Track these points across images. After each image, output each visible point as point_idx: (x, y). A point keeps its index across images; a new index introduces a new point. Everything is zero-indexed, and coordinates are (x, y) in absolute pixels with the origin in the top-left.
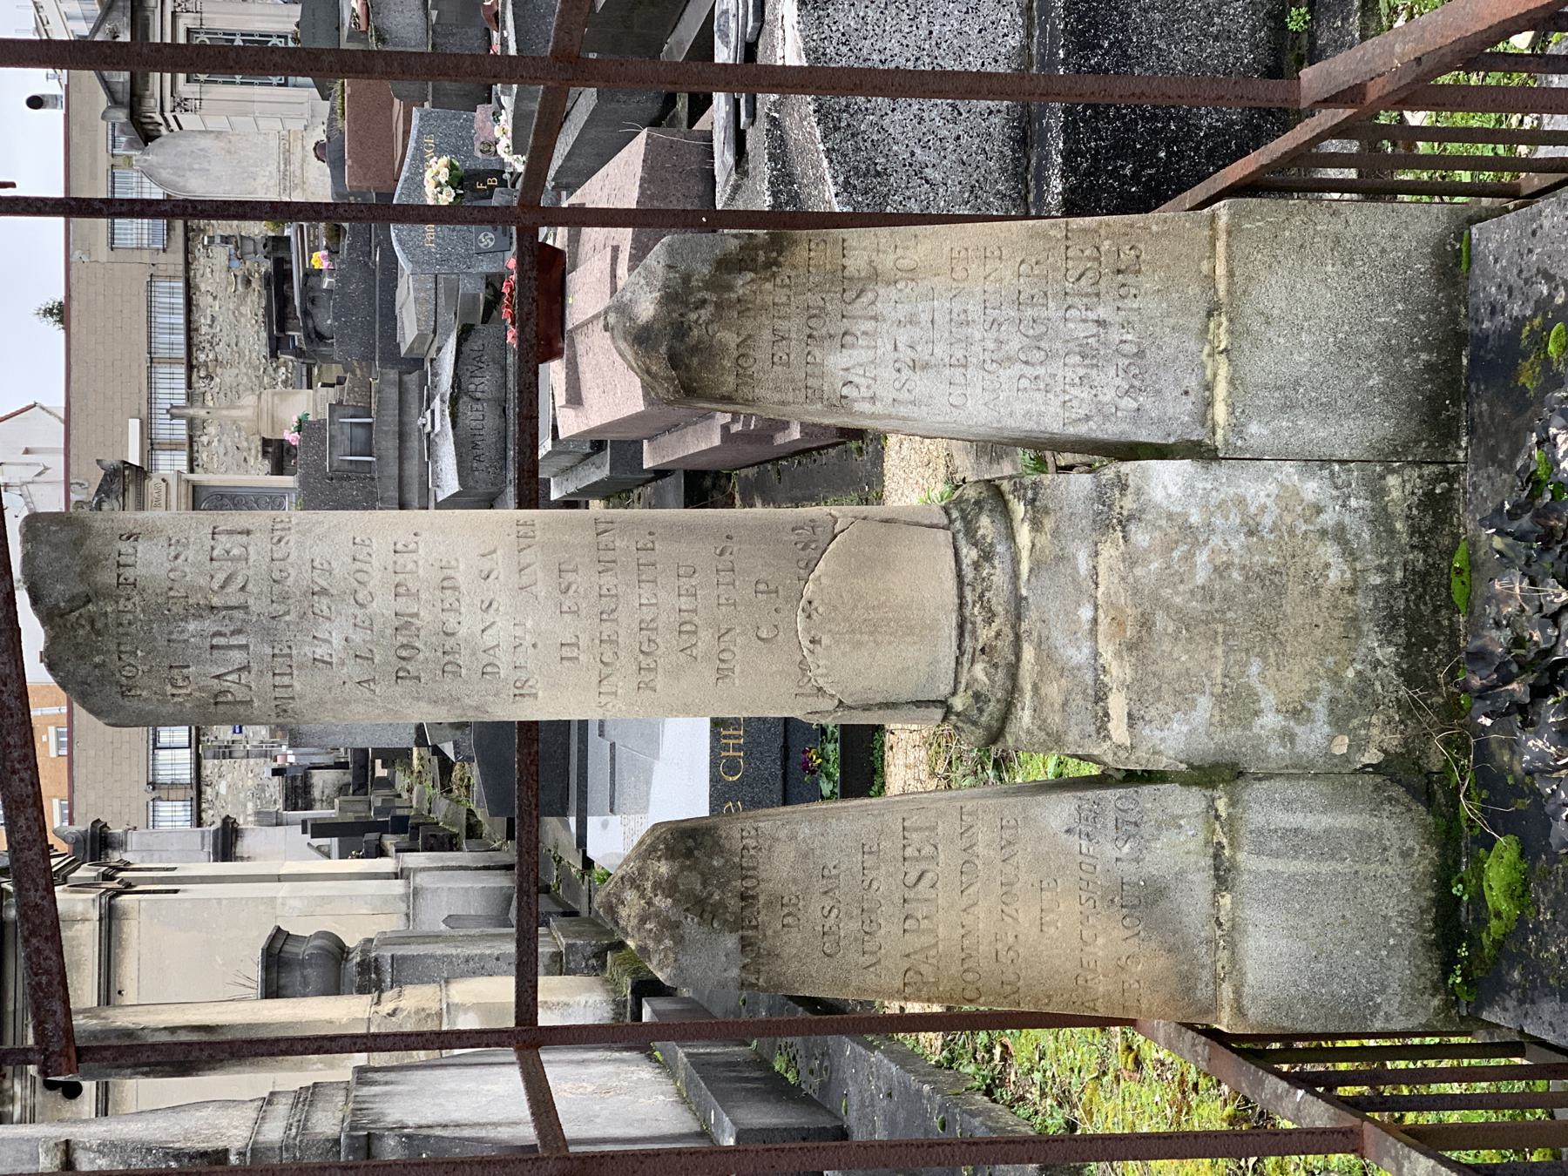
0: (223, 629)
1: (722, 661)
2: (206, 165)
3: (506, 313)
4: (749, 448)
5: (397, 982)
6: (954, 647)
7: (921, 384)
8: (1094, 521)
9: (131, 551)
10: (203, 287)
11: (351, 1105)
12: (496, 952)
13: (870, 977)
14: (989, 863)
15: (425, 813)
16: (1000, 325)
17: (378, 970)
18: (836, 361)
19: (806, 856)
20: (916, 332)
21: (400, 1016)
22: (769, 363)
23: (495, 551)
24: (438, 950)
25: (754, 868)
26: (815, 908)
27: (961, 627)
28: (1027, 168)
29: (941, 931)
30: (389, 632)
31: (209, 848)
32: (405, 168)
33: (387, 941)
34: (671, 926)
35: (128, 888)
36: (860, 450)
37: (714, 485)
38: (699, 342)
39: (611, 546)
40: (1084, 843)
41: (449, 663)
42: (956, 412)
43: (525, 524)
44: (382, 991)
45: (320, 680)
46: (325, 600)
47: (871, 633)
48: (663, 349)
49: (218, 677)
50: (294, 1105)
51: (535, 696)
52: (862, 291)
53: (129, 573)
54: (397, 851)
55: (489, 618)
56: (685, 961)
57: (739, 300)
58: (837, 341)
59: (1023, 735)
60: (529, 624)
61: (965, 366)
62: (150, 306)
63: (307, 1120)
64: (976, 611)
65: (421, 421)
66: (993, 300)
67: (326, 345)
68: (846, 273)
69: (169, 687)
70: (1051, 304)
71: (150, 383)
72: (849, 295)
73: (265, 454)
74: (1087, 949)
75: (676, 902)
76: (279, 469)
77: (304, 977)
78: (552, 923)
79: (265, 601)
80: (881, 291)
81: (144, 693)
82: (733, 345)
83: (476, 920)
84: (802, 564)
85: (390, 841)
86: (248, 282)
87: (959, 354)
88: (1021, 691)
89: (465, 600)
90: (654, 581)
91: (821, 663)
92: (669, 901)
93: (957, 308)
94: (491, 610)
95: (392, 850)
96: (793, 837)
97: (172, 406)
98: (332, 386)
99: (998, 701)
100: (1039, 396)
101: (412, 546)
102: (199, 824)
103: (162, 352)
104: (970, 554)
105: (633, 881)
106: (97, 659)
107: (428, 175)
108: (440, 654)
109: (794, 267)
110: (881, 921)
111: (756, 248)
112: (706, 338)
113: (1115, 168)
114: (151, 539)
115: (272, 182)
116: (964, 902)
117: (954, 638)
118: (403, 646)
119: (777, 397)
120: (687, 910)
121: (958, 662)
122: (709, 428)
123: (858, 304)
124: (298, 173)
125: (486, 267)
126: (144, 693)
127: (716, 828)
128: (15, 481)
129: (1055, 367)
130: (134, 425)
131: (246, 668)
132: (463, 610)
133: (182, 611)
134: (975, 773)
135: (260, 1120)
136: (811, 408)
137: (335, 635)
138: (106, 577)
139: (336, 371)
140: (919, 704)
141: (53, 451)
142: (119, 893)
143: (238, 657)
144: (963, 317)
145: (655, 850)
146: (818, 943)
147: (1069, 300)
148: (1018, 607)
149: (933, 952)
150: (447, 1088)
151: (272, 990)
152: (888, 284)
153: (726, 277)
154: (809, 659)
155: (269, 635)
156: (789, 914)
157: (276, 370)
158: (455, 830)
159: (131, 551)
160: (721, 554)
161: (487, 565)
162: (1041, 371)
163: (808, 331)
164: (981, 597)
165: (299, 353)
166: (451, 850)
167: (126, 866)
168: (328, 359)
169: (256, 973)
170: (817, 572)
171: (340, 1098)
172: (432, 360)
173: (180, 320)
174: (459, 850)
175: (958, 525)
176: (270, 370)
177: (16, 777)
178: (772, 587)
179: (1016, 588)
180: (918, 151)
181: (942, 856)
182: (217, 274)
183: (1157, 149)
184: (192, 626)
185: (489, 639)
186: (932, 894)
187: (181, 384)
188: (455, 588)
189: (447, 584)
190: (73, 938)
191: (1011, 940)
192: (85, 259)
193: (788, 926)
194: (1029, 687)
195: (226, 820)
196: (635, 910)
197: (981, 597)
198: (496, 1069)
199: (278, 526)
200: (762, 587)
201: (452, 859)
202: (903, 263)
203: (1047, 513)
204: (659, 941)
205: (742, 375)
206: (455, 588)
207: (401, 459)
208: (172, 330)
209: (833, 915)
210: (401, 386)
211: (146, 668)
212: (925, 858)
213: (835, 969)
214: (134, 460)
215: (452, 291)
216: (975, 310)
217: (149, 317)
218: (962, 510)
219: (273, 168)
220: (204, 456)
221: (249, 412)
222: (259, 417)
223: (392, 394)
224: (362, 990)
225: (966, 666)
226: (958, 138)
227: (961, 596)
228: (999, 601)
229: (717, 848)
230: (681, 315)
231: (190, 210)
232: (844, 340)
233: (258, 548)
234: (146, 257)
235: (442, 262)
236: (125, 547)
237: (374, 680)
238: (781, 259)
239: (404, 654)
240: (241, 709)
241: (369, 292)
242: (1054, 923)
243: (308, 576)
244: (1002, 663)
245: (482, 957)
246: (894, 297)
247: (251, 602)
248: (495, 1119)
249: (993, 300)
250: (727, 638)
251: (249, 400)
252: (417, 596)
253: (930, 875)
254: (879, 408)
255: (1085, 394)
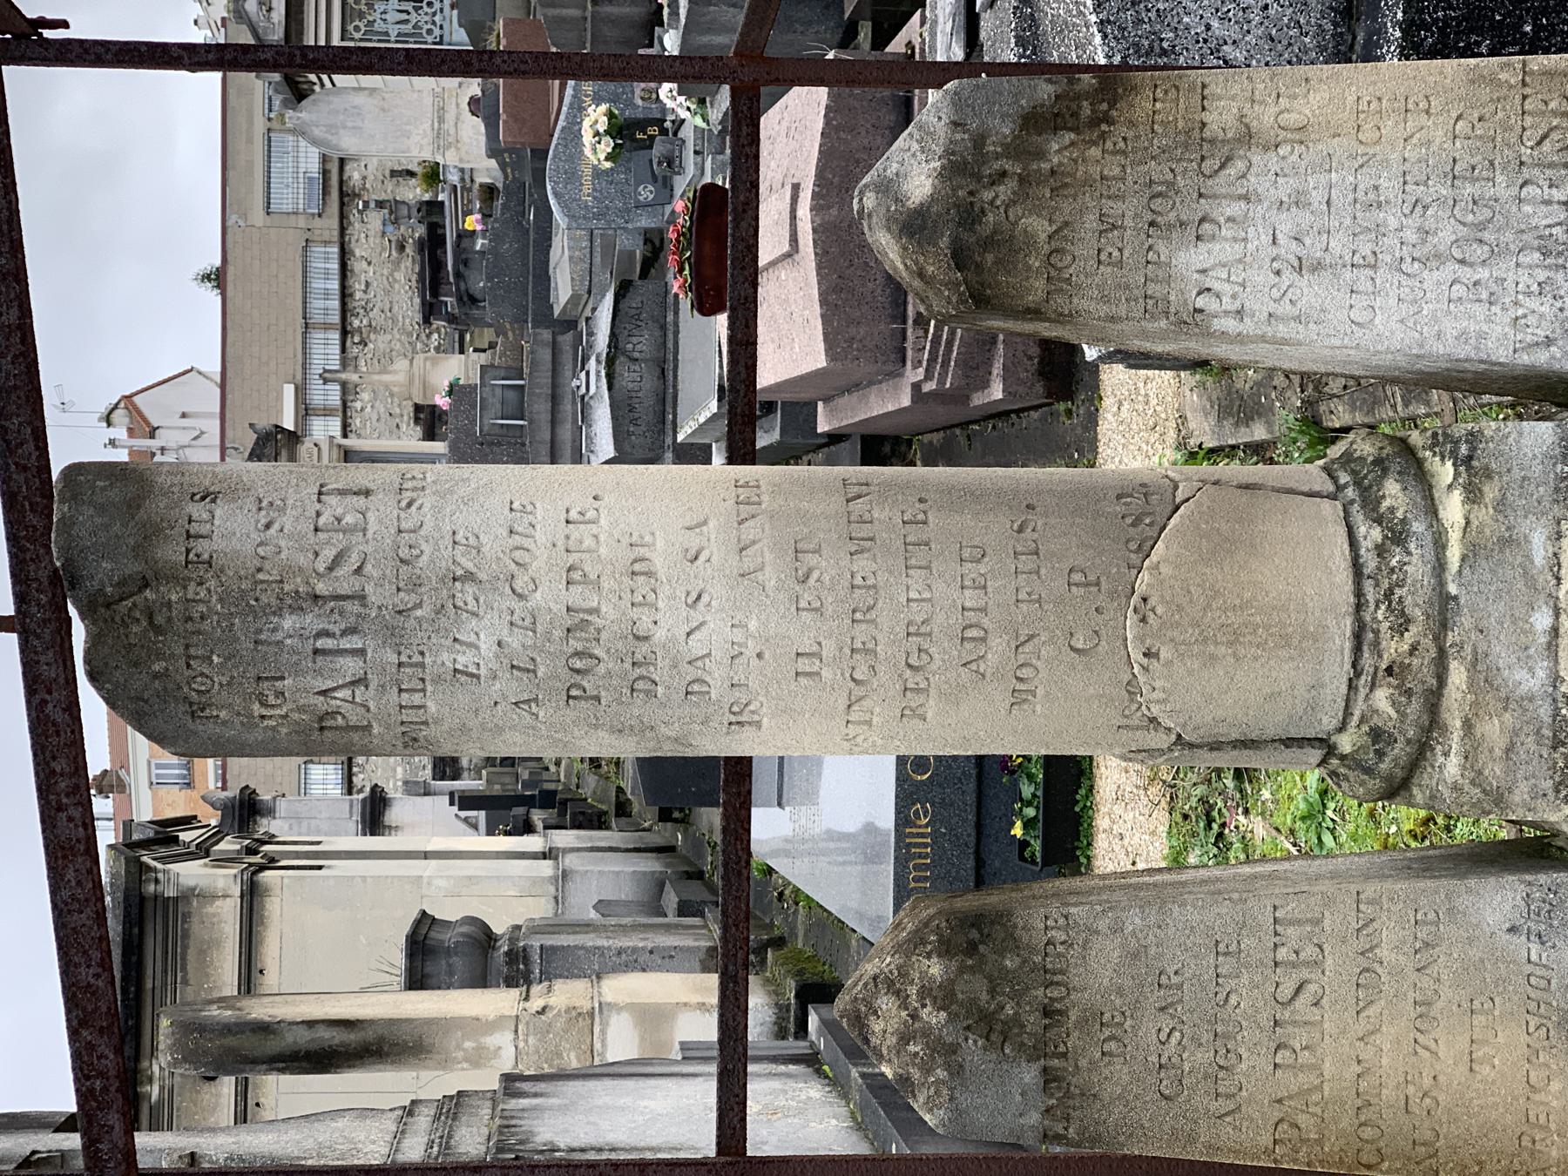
0: (331, 627)
1: (1019, 679)
2: (359, 124)
3: (671, 260)
4: (940, 410)
5: (548, 976)
6: (1348, 666)
7: (1309, 292)
8: (1557, 490)
9: (205, 516)
10: (358, 253)
11: (498, 1121)
12: (650, 945)
13: (1226, 1130)
14: (1397, 973)
15: (573, 787)
16: (1425, 208)
17: (526, 960)
18: (1189, 259)
19: (1136, 956)
20: (1305, 218)
21: (550, 1014)
22: (1093, 262)
23: (705, 523)
24: (590, 940)
25: (1062, 972)
26: (1149, 1029)
27: (1358, 637)
28: (1352, 47)
29: (1328, 1068)
30: (558, 633)
31: (357, 817)
32: (562, 117)
33: (538, 929)
34: (944, 1051)
35: (271, 863)
36: (1069, 413)
37: (893, 451)
38: (995, 232)
39: (867, 517)
40: (1535, 948)
41: (641, 678)
42: (1359, 332)
43: (747, 485)
44: (529, 983)
45: (463, 698)
46: (470, 589)
47: (1230, 644)
48: (944, 242)
49: (324, 693)
50: (436, 1118)
51: (758, 724)
52: (1229, 159)
53: (202, 547)
54: (546, 828)
55: (696, 617)
56: (964, 1100)
57: (1053, 172)
58: (1191, 231)
59: (1446, 793)
60: (753, 625)
61: (1374, 267)
62: (305, 272)
63: (450, 1137)
64: (1380, 615)
65: (575, 383)
66: (1416, 173)
67: (478, 308)
68: (1207, 134)
69: (256, 707)
70: (1500, 179)
71: (304, 348)
72: (1210, 165)
73: (417, 420)
74: (1537, 1097)
75: (953, 1017)
76: (430, 435)
77: (450, 965)
78: (708, 915)
79: (390, 588)
80: (1256, 159)
81: (223, 714)
82: (1043, 236)
83: (626, 903)
84: (1133, 546)
85: (537, 817)
86: (401, 248)
87: (1366, 250)
88: (1444, 730)
89: (664, 591)
90: (928, 568)
91: (1157, 684)
92: (943, 1015)
93: (1365, 182)
94: (701, 605)
95: (540, 825)
96: (1117, 929)
97: (326, 371)
98: (484, 351)
99: (1409, 742)
100: (1480, 310)
101: (591, 514)
102: (350, 793)
103: (316, 317)
104: (1371, 535)
105: (890, 983)
106: (157, 667)
107: (586, 123)
108: (627, 666)
109: (1132, 124)
110: (1242, 1051)
111: (1078, 97)
112: (1006, 226)
113: (1468, 45)
114: (234, 500)
115: (425, 142)
116: (1361, 1028)
117: (1347, 652)
118: (577, 654)
119: (1104, 310)
120: (968, 1028)
121: (1351, 686)
122: (897, 388)
123: (1222, 178)
124: (452, 131)
125: (645, 221)
126: (223, 714)
127: (1010, 914)
128: (173, 445)
129: (1504, 268)
130: (289, 390)
131: (362, 681)
132: (661, 604)
133: (274, 602)
134: (1210, 781)
135: (400, 1134)
136: (1150, 326)
137: (484, 638)
138: (171, 553)
139: (488, 335)
140: (1289, 742)
141: (209, 415)
142: (262, 868)
143: (351, 666)
144: (1371, 196)
145: (924, 942)
146: (1151, 1080)
147: (1526, 173)
148: (1443, 610)
149: (1316, 1097)
150: (600, 1102)
151: (416, 980)
152: (1266, 149)
153: (1035, 138)
154: (1141, 679)
155: (393, 635)
156: (1112, 1038)
157: (428, 336)
158: (604, 807)
159: (205, 516)
160: (1020, 531)
161: (694, 541)
162: (1483, 274)
163: (1149, 217)
164: (1389, 594)
165: (451, 319)
166: (600, 828)
167: (270, 839)
168: (482, 323)
169: (399, 959)
170: (1154, 557)
171: (486, 1112)
172: (588, 319)
173: (335, 285)
174: (608, 828)
175: (1350, 493)
176: (423, 336)
177: (63, 815)
178: (1092, 578)
179: (1441, 584)
180: (1215, 24)
181: (1329, 961)
182: (371, 240)
183: (1523, 22)
184: (288, 622)
185: (697, 646)
186: (1315, 1015)
187: (337, 350)
188: (649, 574)
189: (639, 569)
190: (214, 915)
191: (1427, 1082)
192: (241, 223)
193: (1111, 1054)
194: (1458, 724)
195: (375, 788)
196: (894, 1025)
197: (1389, 594)
198: (652, 1082)
199: (408, 485)
200: (1077, 577)
201: (601, 839)
202: (1291, 119)
203: (1489, 477)
204: (927, 1070)
205: (1057, 281)
206: (649, 574)
207: (554, 423)
208: (326, 295)
209: (1173, 1041)
210: (555, 347)
211: (224, 680)
212: (1306, 964)
213: (1175, 1117)
214: (289, 425)
215: (608, 247)
216: (1389, 186)
217: (305, 282)
218: (1354, 473)
219: (427, 126)
220: (358, 421)
221: (401, 378)
222: (411, 381)
223: (546, 355)
224: (510, 983)
225: (1363, 692)
226: (1266, 7)
227: (1359, 593)
228: (1416, 602)
229: (1012, 942)
230: (971, 193)
231: (298, 60)
232: (1199, 230)
233: (381, 515)
234: (302, 222)
235: (597, 216)
236: (198, 510)
237: (536, 700)
238: (1115, 113)
239: (578, 664)
240: (356, 737)
241: (523, 251)
242: (1488, 1060)
243: (447, 553)
244: (1419, 689)
245: (635, 950)
246: (1275, 168)
247: (369, 589)
248: (654, 1144)
249: (1416, 173)
250: (1028, 648)
251: (401, 365)
252: (597, 585)
253: (1312, 988)
254: (1248, 327)
255: (1546, 307)
